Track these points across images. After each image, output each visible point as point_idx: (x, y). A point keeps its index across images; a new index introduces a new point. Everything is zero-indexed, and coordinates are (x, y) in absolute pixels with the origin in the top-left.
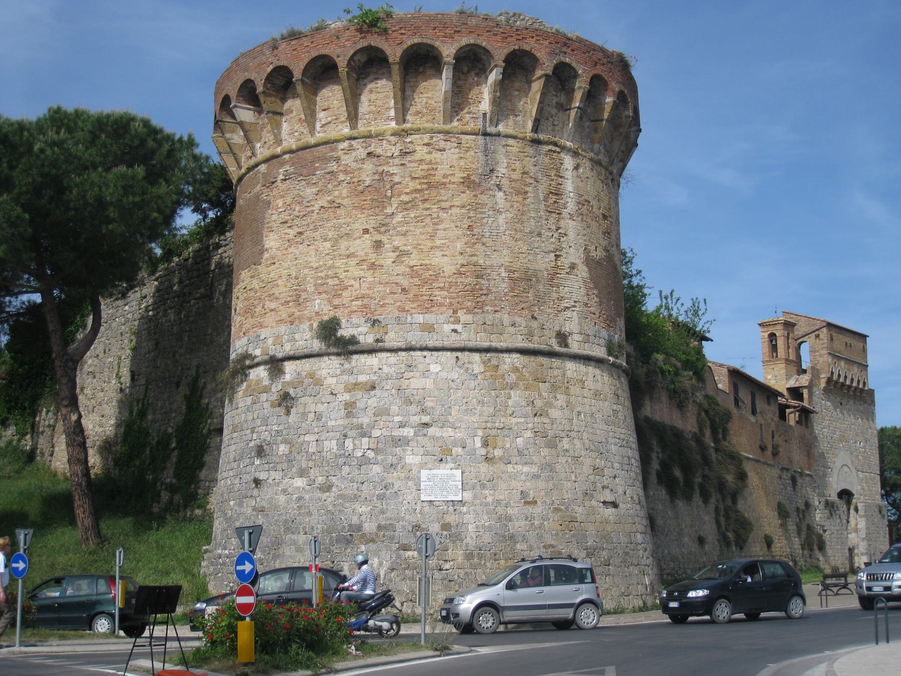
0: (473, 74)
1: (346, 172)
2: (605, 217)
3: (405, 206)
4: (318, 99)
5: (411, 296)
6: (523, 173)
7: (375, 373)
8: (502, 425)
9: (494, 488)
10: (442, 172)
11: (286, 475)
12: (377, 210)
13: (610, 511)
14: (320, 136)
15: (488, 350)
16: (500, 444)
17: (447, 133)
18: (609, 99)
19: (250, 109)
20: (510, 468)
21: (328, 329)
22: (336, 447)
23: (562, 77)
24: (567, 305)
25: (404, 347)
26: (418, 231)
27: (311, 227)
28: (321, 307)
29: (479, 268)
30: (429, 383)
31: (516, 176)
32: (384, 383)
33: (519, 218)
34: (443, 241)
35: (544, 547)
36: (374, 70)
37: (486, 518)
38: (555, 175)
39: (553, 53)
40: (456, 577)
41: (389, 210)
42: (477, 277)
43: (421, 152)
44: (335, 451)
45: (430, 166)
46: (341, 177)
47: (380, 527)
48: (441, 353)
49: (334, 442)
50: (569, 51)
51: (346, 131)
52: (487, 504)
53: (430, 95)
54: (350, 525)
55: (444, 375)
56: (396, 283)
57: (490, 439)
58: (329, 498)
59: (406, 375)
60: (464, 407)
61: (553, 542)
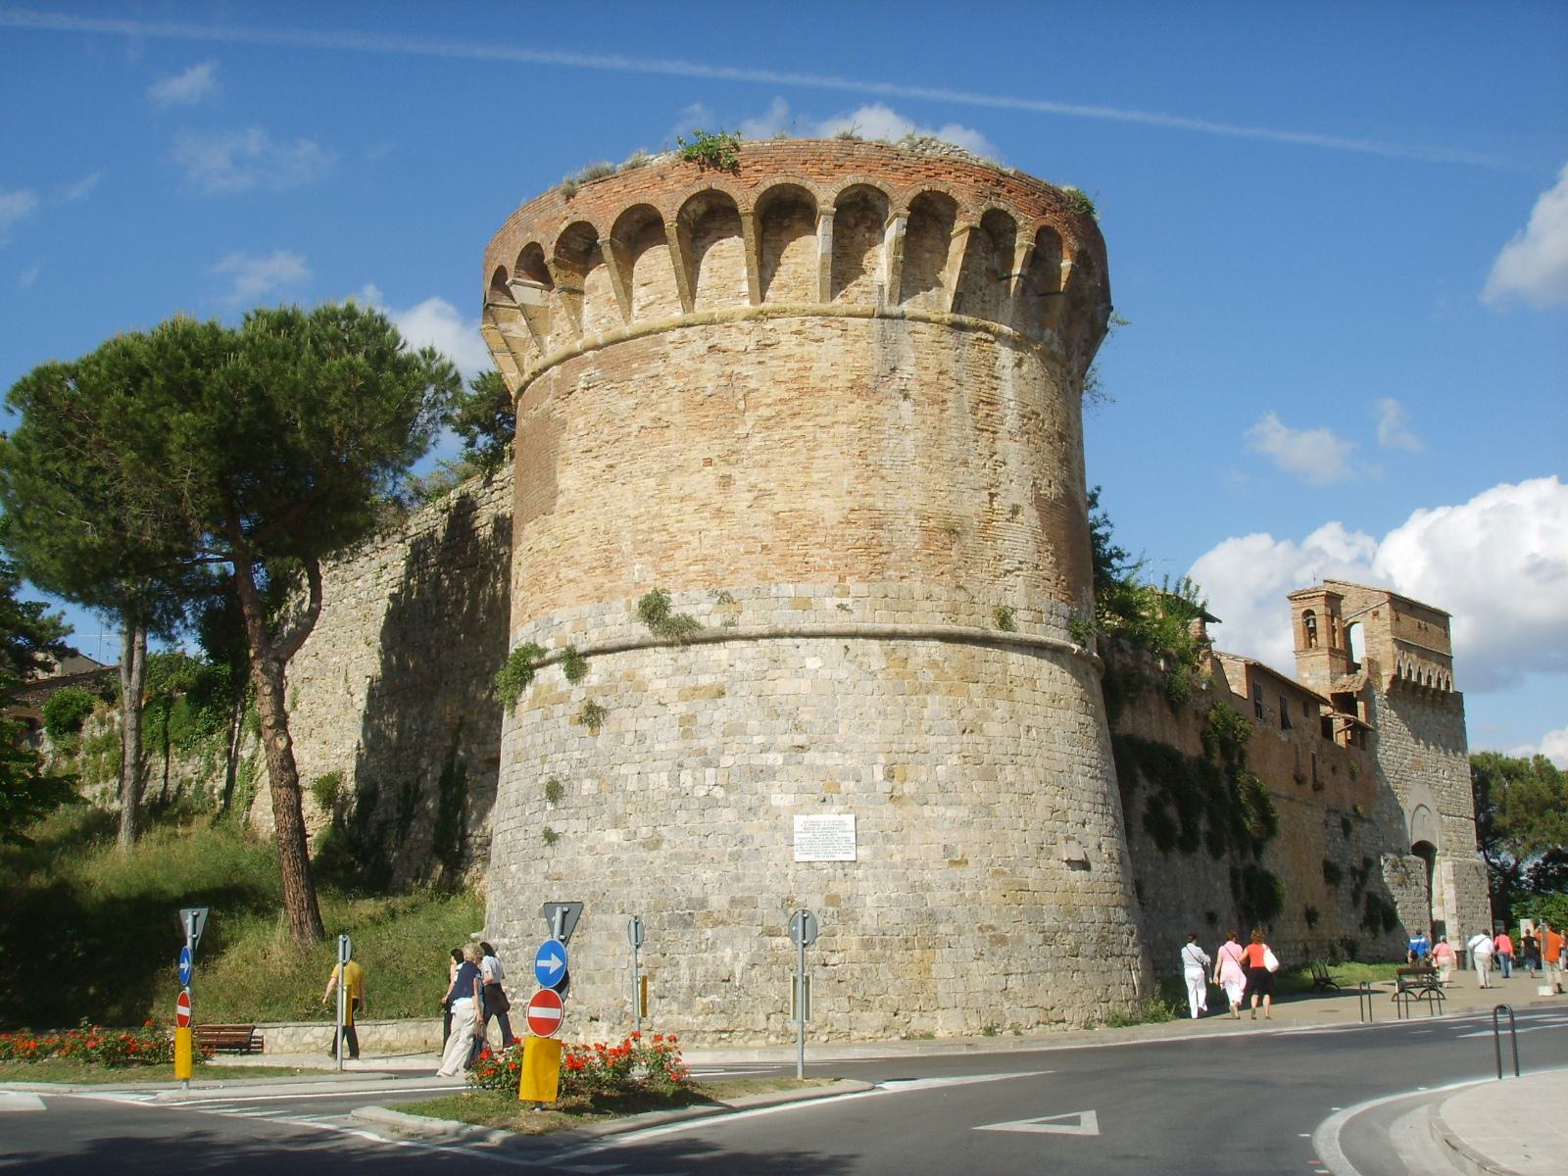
0: (862, 228)
1: (677, 375)
2: (1062, 437)
3: (767, 424)
4: (635, 269)
5: (775, 556)
6: (940, 373)
7: (724, 671)
9: (904, 841)
12: (724, 431)
14: (638, 323)
15: (892, 636)
18: (1066, 264)
19: (535, 287)
20: (927, 811)
21: (654, 609)
22: (666, 783)
26: (785, 460)
28: (641, 576)
29: (876, 514)
30: (804, 686)
31: (929, 376)
32: (737, 687)
33: (936, 438)
34: (822, 475)
35: (980, 929)
36: (717, 225)
37: (891, 886)
38: (987, 375)
39: (980, 196)
40: (848, 976)
41: (741, 431)
42: (875, 527)
43: (788, 344)
47: (733, 902)
48: (821, 640)
49: (664, 776)
50: (1004, 191)
51: (678, 315)
52: (893, 866)
53: (799, 260)
54: (689, 899)
55: (826, 673)
58: (658, 857)
60: (856, 721)
61: (992, 922)
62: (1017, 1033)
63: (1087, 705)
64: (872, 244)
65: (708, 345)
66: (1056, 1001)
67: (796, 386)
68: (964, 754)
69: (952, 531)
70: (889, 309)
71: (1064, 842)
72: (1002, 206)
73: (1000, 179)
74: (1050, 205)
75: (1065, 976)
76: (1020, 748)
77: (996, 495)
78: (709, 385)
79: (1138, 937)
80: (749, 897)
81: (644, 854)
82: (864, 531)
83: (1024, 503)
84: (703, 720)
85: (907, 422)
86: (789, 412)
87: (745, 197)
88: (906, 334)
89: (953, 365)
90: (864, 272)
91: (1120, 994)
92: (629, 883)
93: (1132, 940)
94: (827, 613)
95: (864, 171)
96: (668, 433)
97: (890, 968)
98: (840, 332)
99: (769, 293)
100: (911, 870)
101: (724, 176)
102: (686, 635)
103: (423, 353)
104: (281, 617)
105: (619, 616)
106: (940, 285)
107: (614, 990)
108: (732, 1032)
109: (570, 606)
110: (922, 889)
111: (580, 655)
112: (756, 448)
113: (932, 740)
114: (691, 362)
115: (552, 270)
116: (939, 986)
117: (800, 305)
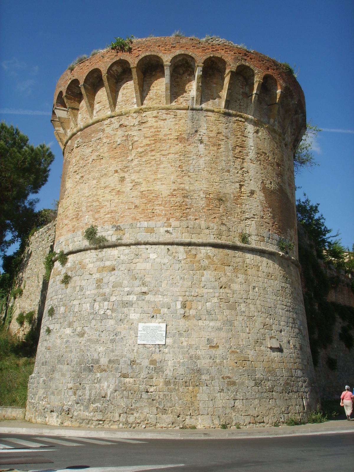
0: (186, 75)
1: (107, 137)
2: (278, 165)
3: (141, 155)
4: (96, 97)
5: (140, 210)
6: (218, 133)
7: (116, 260)
8: (196, 294)
9: (188, 336)
10: (164, 133)
11: (62, 326)
12: (123, 159)
13: (276, 354)
14: (95, 118)
15: (189, 244)
16: (194, 306)
17: (168, 109)
18: (279, 91)
19: (64, 110)
20: (200, 323)
21: (91, 234)
22: (89, 308)
23: (242, 75)
24: (247, 216)
25: (133, 242)
26: (147, 169)
27: (87, 172)
28: (87, 220)
29: (185, 192)
30: (148, 266)
31: (213, 134)
32: (120, 266)
33: (214, 160)
34: (162, 175)
35: (223, 378)
36: (126, 76)
37: (181, 356)
38: (241, 135)
39: (236, 59)
40: (157, 397)
41: (130, 158)
42: (184, 197)
43: (151, 121)
44: (88, 310)
45: (156, 130)
46: (105, 140)
47: (110, 361)
48: (158, 246)
49: (88, 305)
50: (249, 59)
51: (109, 113)
52: (182, 347)
53: (158, 88)
54: (92, 360)
55: (158, 260)
56: (132, 202)
57: (188, 304)
58: (83, 340)
59: (134, 261)
60: (170, 282)
61: (229, 375)
62: (238, 428)
63: (287, 279)
64: (190, 81)
65: (119, 124)
66: (260, 413)
67: (153, 139)
68: (220, 298)
69: (220, 200)
70: (195, 106)
71: (269, 339)
72: (247, 64)
73: (246, 54)
74: (271, 66)
75: (265, 401)
76: (249, 296)
77: (243, 185)
78: (119, 140)
79: (308, 383)
80: (117, 359)
81: (78, 339)
82: (179, 199)
83: (257, 190)
84: (105, 281)
85: (201, 153)
86: (150, 149)
87: (133, 61)
88: (203, 117)
89: (224, 130)
90: (186, 92)
91: (295, 410)
92: (71, 351)
93: (304, 385)
94: (161, 235)
95: (184, 49)
96: (102, 161)
97: (177, 395)
98: (173, 116)
99: (145, 102)
100: (191, 350)
101: (126, 54)
102: (101, 244)
103: (41, 146)
104: (23, 256)
105: (79, 237)
106: (220, 97)
107: (61, 398)
108: (104, 421)
109: (65, 235)
110: (195, 358)
111: (65, 255)
112: (135, 165)
113: (205, 291)
114: (112, 132)
115: (65, 100)
116: (200, 404)
117: (157, 105)
